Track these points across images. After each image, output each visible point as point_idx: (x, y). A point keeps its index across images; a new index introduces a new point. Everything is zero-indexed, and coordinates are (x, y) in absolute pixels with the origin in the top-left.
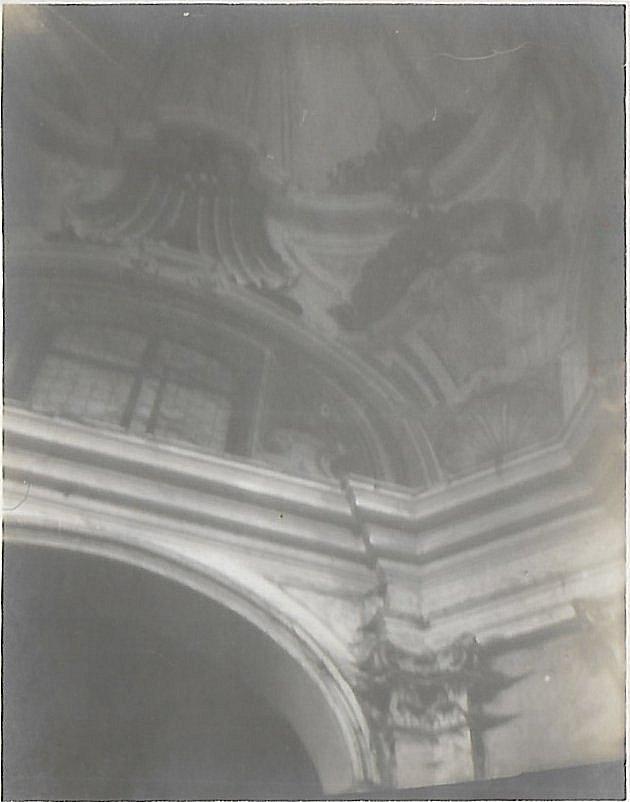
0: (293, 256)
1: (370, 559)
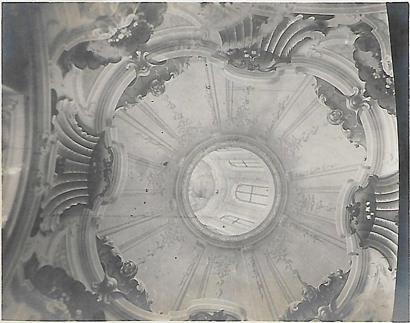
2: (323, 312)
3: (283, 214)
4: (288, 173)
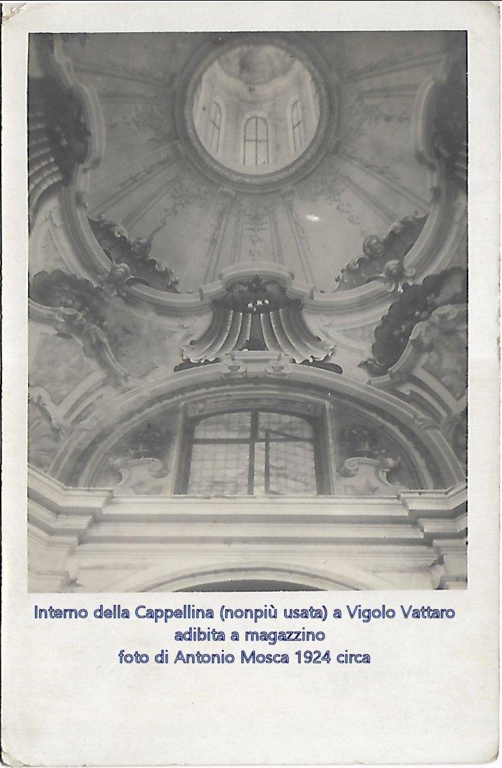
0: (328, 336)
1: (428, 541)
2: (122, 270)
3: (236, 191)
4: (292, 190)
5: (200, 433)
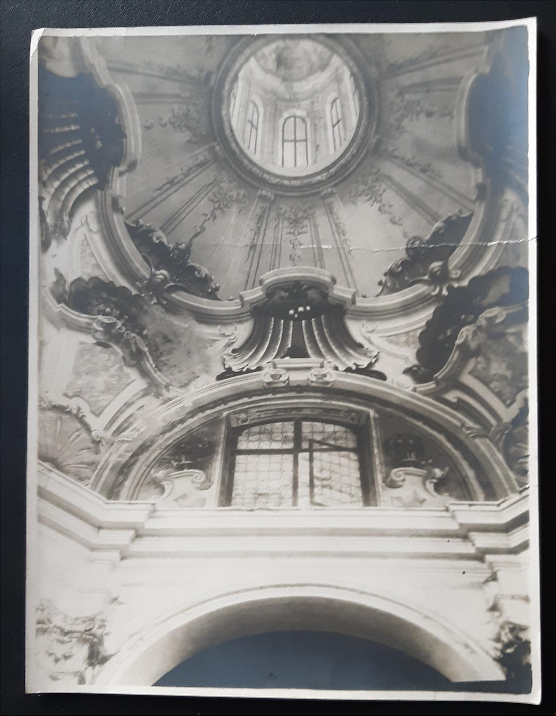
0: (371, 342)
1: (480, 556)
5: (243, 445)
